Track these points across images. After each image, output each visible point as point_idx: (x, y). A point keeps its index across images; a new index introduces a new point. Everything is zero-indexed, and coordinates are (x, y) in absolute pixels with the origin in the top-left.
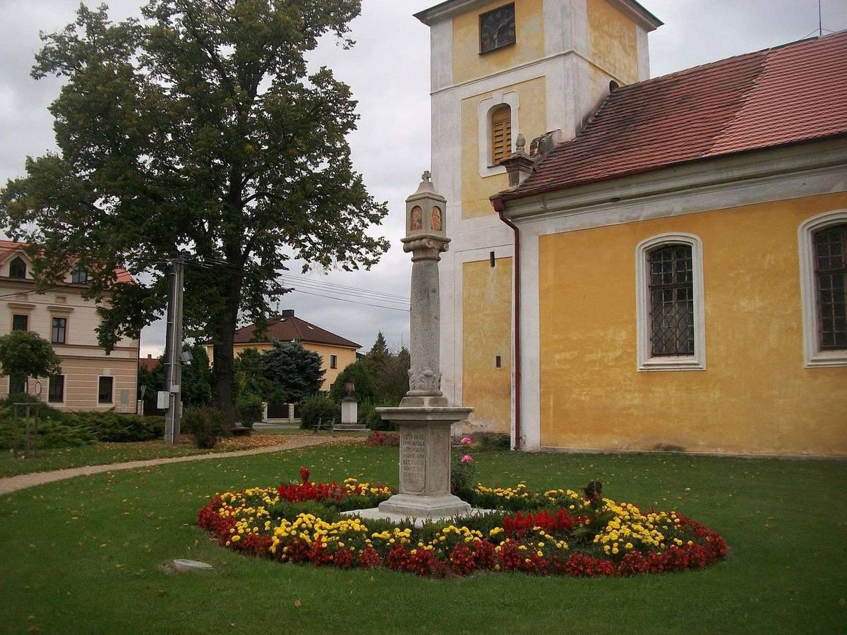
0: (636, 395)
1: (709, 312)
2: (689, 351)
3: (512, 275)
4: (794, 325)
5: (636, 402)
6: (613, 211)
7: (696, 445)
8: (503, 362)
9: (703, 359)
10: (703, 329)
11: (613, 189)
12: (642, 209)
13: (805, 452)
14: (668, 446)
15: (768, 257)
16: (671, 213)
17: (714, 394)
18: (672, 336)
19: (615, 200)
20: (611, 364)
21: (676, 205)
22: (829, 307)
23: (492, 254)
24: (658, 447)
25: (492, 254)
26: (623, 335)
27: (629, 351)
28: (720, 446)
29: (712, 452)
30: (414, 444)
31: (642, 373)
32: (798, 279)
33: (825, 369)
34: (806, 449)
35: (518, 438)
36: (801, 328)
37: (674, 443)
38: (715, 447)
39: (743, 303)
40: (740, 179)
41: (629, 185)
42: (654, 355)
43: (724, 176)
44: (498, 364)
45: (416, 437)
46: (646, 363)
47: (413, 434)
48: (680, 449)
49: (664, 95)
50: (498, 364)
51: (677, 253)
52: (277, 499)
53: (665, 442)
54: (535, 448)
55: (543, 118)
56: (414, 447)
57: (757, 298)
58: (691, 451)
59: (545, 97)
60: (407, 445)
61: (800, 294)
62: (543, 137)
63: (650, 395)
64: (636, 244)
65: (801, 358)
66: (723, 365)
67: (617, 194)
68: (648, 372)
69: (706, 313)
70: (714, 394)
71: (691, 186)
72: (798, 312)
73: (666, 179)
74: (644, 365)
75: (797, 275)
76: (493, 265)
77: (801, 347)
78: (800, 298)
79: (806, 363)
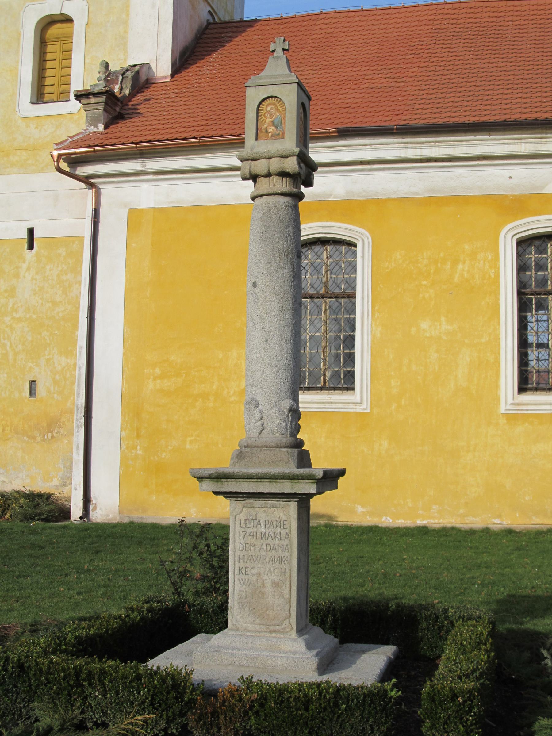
1: (378, 335)
2: (346, 382)
3: (80, 262)
8: (41, 390)
9: (367, 396)
13: (497, 521)
15: (460, 266)
16: (331, 195)
17: (380, 445)
20: (232, 399)
23: (31, 231)
25: (31, 231)
32: (497, 299)
33: (526, 417)
35: (87, 500)
40: (429, 160)
43: (411, 153)
44: (32, 392)
48: (330, 517)
50: (32, 392)
51: (537, 248)
52: (189, 728)
54: (111, 516)
55: (123, 43)
56: (264, 542)
57: (443, 319)
59: (128, 15)
60: (249, 540)
62: (127, 70)
69: (373, 336)
70: (380, 445)
73: (526, 134)
76: (31, 246)
78: (499, 323)
79: (503, 409)
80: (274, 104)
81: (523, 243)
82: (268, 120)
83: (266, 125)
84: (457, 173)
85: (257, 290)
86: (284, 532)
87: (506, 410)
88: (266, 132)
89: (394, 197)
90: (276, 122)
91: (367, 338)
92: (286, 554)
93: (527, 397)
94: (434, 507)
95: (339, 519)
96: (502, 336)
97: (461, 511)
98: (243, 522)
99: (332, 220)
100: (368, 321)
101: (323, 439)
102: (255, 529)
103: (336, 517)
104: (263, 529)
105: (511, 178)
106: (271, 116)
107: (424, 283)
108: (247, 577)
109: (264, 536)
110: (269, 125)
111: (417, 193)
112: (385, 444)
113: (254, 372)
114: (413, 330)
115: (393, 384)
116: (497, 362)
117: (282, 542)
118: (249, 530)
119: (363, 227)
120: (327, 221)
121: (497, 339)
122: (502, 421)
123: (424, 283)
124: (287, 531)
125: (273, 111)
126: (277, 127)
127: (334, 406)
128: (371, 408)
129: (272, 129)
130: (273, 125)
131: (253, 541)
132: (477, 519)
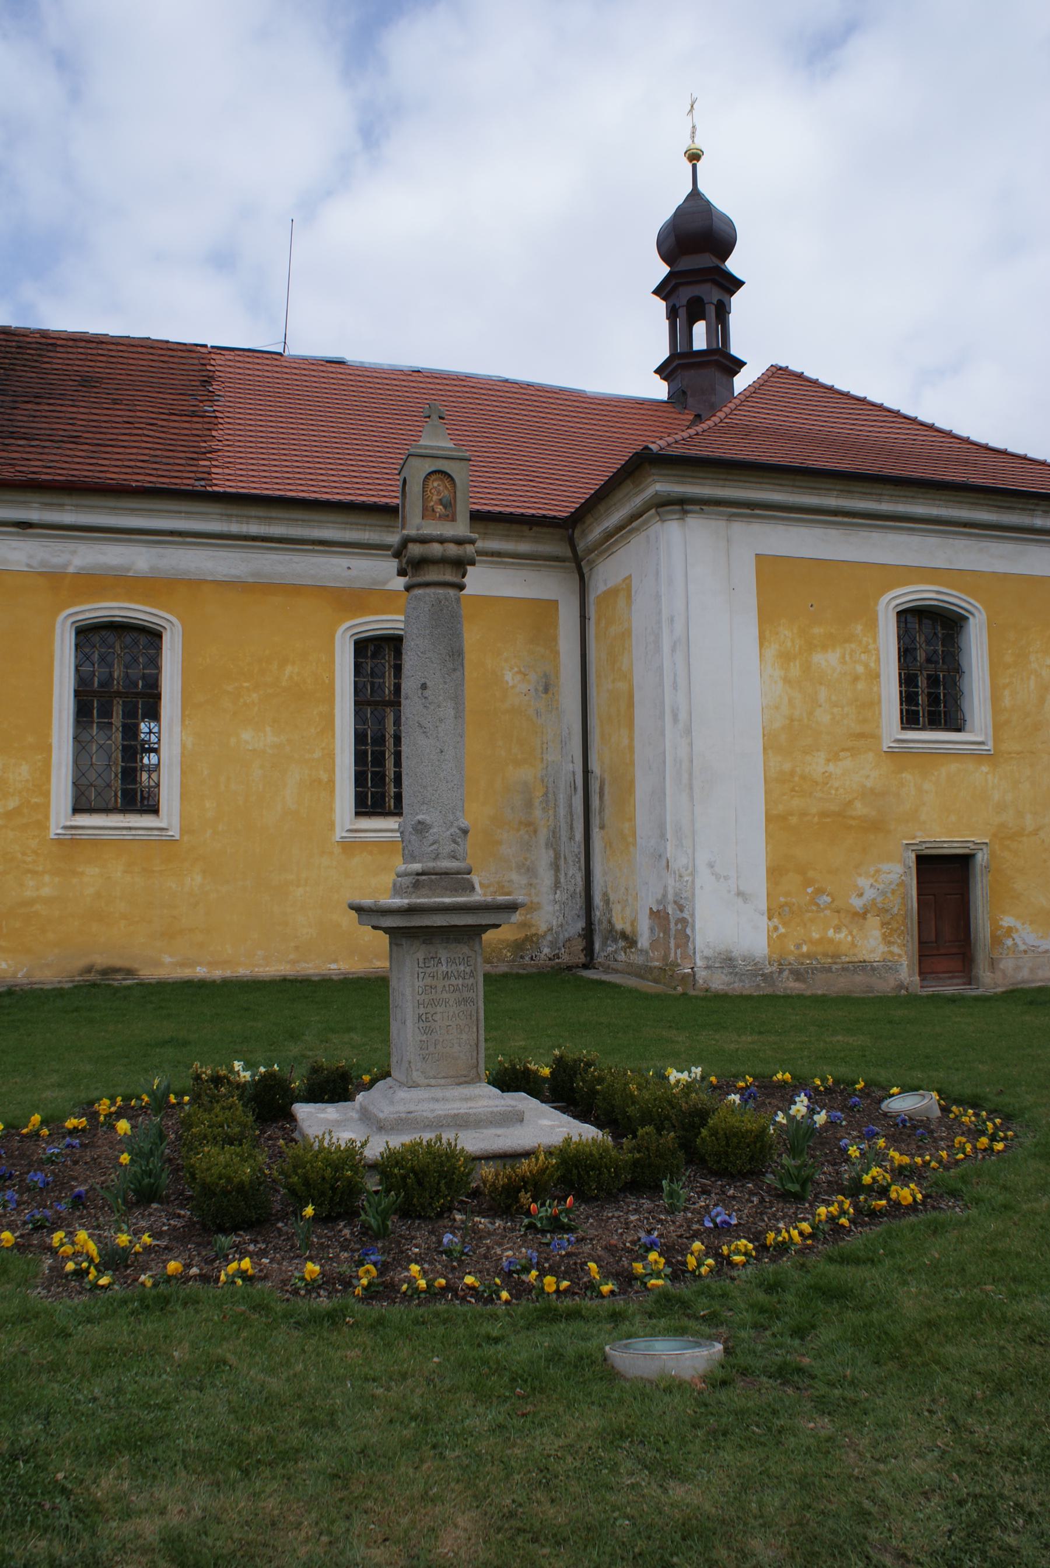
0: (47, 878)
1: (189, 746)
4: (324, 777)
5: (46, 891)
6: (14, 544)
7: (158, 964)
9: (176, 821)
10: (177, 772)
11: (25, 504)
12: (74, 553)
13: (333, 966)
14: (109, 968)
15: (289, 669)
18: (120, 782)
19: (24, 525)
21: (139, 558)
22: (365, 752)
24: (89, 970)
26: (23, 772)
27: (34, 800)
28: (200, 964)
29: (186, 973)
30: (446, 976)
31: (59, 841)
32: (333, 708)
33: (364, 845)
34: (335, 961)
36: (333, 782)
37: (118, 963)
38: (193, 964)
39: (246, 735)
41: (63, 505)
42: (76, 810)
43: (235, 528)
45: (451, 961)
46: (69, 823)
47: (443, 955)
49: (39, 355)
53: (101, 961)
56: (447, 983)
57: (268, 729)
58: (150, 973)
60: (428, 981)
61: (333, 730)
63: (75, 881)
64: (57, 614)
65: (332, 826)
66: (209, 831)
67: (34, 515)
68: (72, 844)
69: (183, 746)
71: (172, 533)
72: (330, 756)
74: (65, 828)
75: (330, 700)
77: (332, 810)
78: (333, 736)
79: (339, 833)
80: (442, 480)
81: (85, 633)
82: (435, 498)
83: (432, 504)
84: (287, 557)
85: (427, 693)
86: (468, 970)
87: (342, 838)
88: (433, 510)
89: (210, 578)
90: (444, 501)
91: (177, 750)
92: (471, 994)
93: (366, 823)
94: (259, 953)
95: (141, 973)
96: (338, 751)
97: (292, 956)
98: (421, 961)
99: (130, 600)
100: (177, 729)
101: (119, 874)
102: (435, 969)
103: (137, 970)
104: (444, 968)
105: (349, 568)
106: (439, 493)
107: (246, 684)
108: (428, 1024)
109: (446, 976)
110: (436, 503)
111: (239, 577)
112: (199, 879)
113: (425, 787)
114: (233, 740)
115: (208, 805)
116: (331, 781)
117: (466, 981)
118: (429, 970)
119: (169, 611)
120: (124, 601)
121: (331, 756)
122: (337, 850)
123: (246, 684)
124: (472, 968)
125: (441, 488)
126: (445, 507)
127: (133, 832)
128: (181, 835)
129: (439, 509)
130: (441, 504)
131: (434, 983)
132: (310, 965)
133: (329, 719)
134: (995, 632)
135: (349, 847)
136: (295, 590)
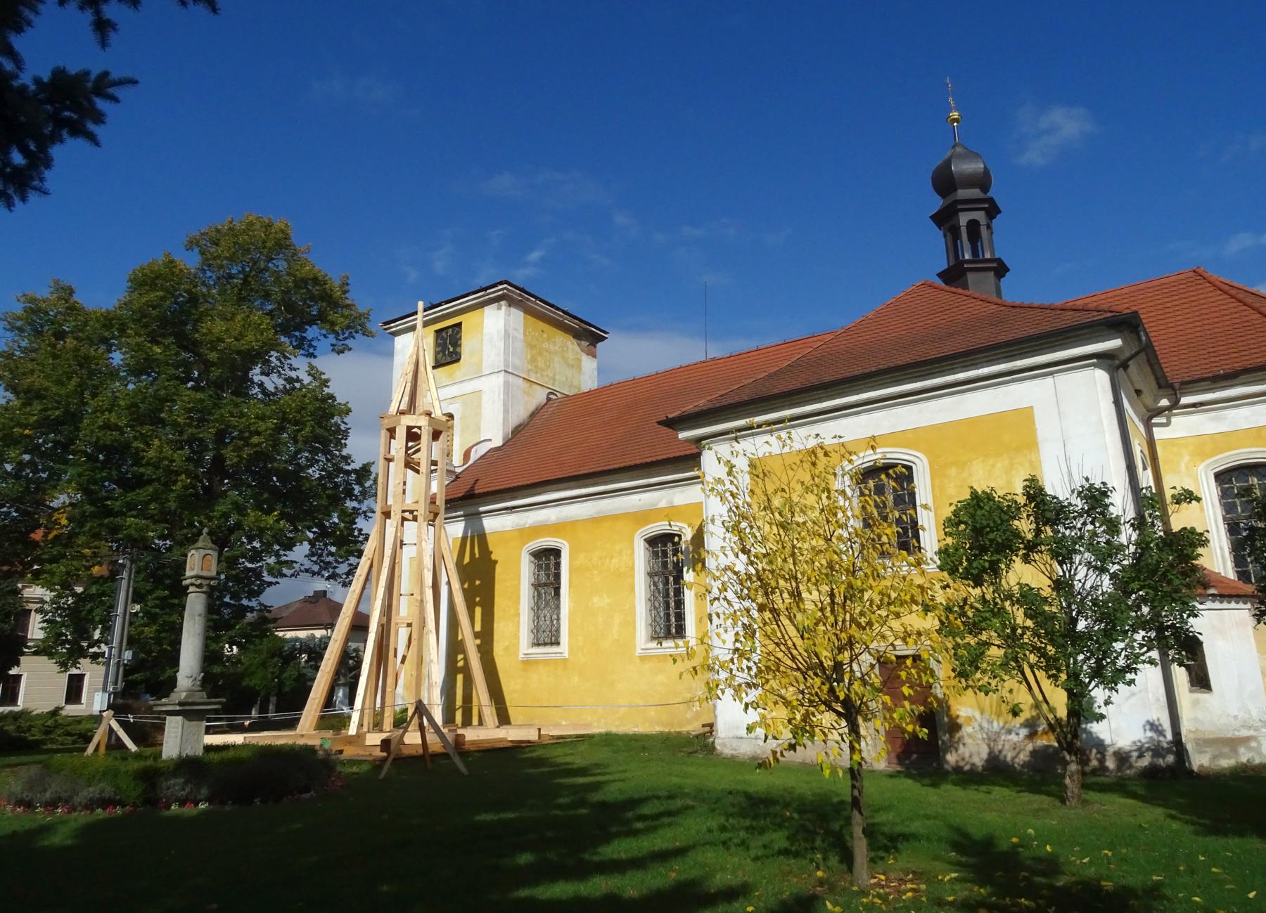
33: (650, 658)
55: (478, 429)
133: (632, 588)
134: (937, 472)
135: (643, 659)
136: (615, 517)
